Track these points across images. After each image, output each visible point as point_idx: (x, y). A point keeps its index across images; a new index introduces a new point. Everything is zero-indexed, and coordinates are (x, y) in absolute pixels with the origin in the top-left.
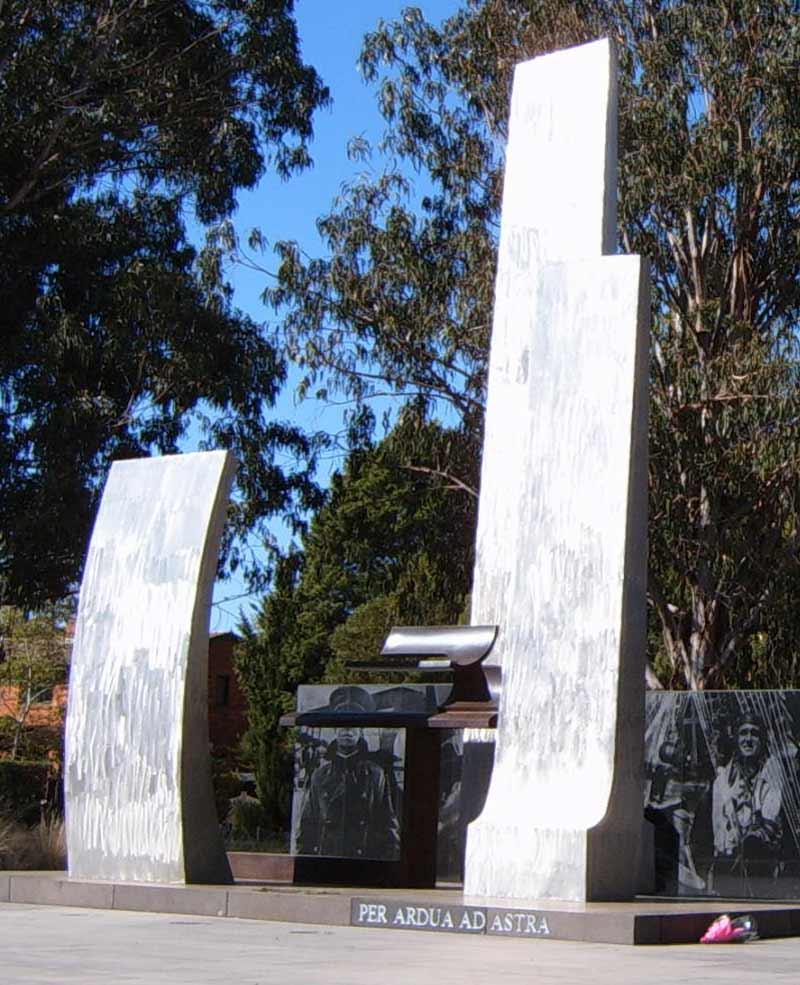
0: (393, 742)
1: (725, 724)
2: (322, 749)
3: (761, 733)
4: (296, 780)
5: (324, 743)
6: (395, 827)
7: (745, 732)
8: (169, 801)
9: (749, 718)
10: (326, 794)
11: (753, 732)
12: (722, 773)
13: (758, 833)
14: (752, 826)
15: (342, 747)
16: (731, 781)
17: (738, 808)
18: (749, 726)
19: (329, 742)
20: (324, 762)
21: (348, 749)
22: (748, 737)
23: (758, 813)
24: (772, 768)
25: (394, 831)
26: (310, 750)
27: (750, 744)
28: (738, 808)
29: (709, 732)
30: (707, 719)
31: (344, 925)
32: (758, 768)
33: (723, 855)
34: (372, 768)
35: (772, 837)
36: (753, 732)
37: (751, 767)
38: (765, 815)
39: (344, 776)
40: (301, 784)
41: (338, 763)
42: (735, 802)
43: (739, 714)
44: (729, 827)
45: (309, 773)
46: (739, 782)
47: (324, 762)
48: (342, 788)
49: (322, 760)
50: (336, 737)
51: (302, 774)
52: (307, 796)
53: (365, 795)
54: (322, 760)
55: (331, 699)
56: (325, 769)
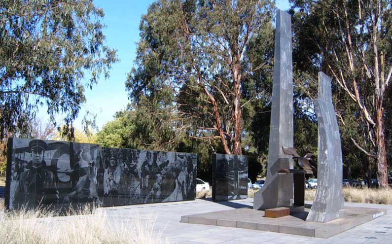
0: (56, 162)
1: (107, 157)
2: (25, 164)
3: (115, 160)
4: (12, 177)
5: (26, 162)
6: (57, 194)
7: (112, 159)
8: (305, 194)
9: (113, 155)
10: (27, 183)
11: (114, 159)
12: (106, 170)
13: (115, 187)
14: (113, 186)
15: (35, 164)
16: (108, 173)
17: (110, 180)
18: (113, 158)
19: (29, 162)
20: (26, 170)
21: (38, 165)
22: (113, 161)
23: (115, 182)
24: (118, 170)
25: (57, 195)
26: (20, 165)
27: (113, 162)
28: (110, 180)
29: (103, 159)
30: (102, 155)
31: (233, 227)
32: (115, 169)
33: (106, 194)
34: (48, 172)
35: (118, 188)
36: (114, 159)
37: (114, 168)
38: (116, 182)
39: (35, 175)
40: (14, 179)
41: (32, 170)
42: (109, 179)
43: (111, 154)
44: (108, 186)
45: (19, 174)
46: (110, 173)
47: (26, 170)
48: (34, 180)
49: (25, 169)
50: (32, 160)
51: (15, 174)
52: (18, 183)
53: (45, 182)
54: (25, 169)
55: (29, 144)
56: (27, 172)
